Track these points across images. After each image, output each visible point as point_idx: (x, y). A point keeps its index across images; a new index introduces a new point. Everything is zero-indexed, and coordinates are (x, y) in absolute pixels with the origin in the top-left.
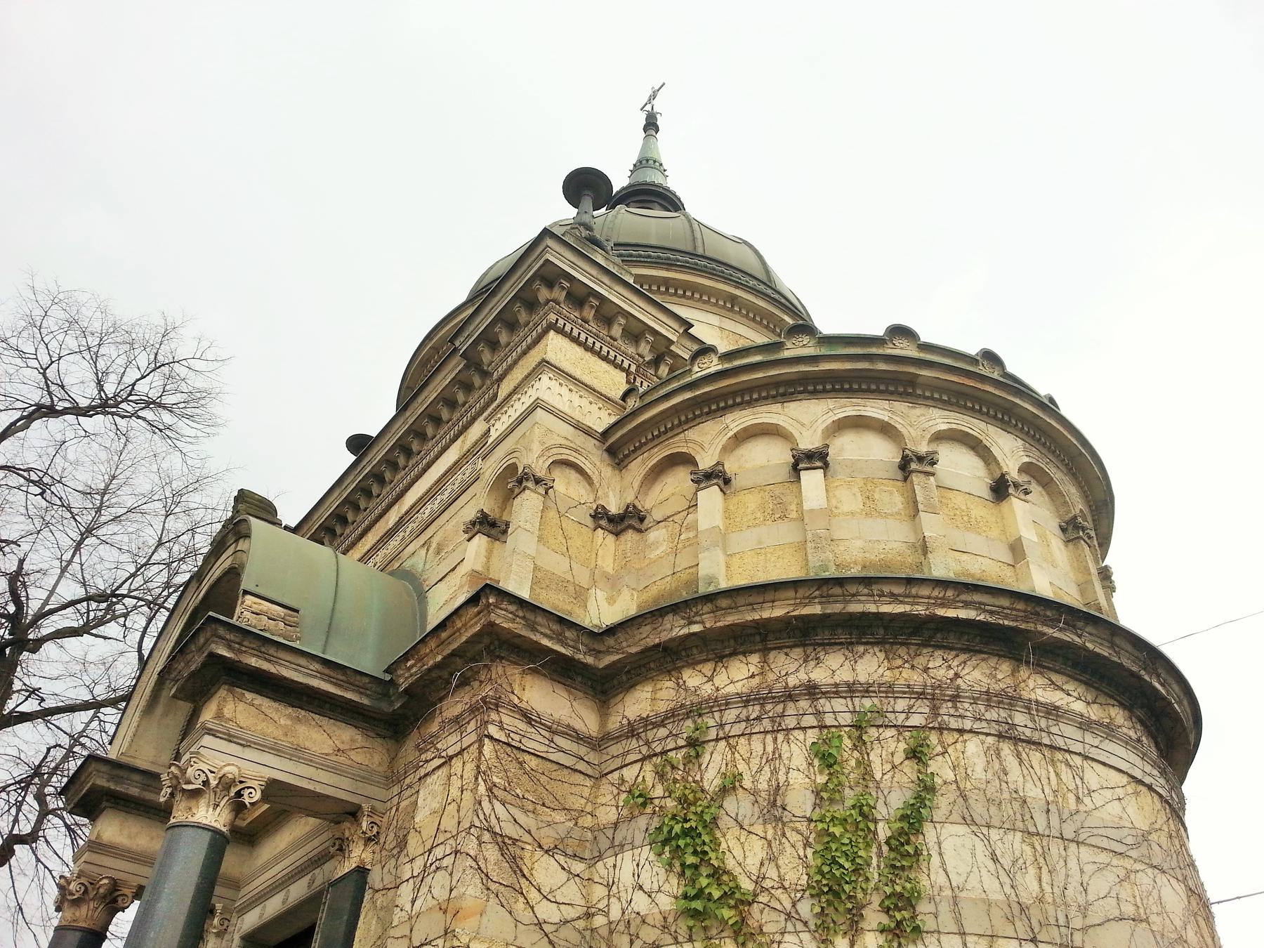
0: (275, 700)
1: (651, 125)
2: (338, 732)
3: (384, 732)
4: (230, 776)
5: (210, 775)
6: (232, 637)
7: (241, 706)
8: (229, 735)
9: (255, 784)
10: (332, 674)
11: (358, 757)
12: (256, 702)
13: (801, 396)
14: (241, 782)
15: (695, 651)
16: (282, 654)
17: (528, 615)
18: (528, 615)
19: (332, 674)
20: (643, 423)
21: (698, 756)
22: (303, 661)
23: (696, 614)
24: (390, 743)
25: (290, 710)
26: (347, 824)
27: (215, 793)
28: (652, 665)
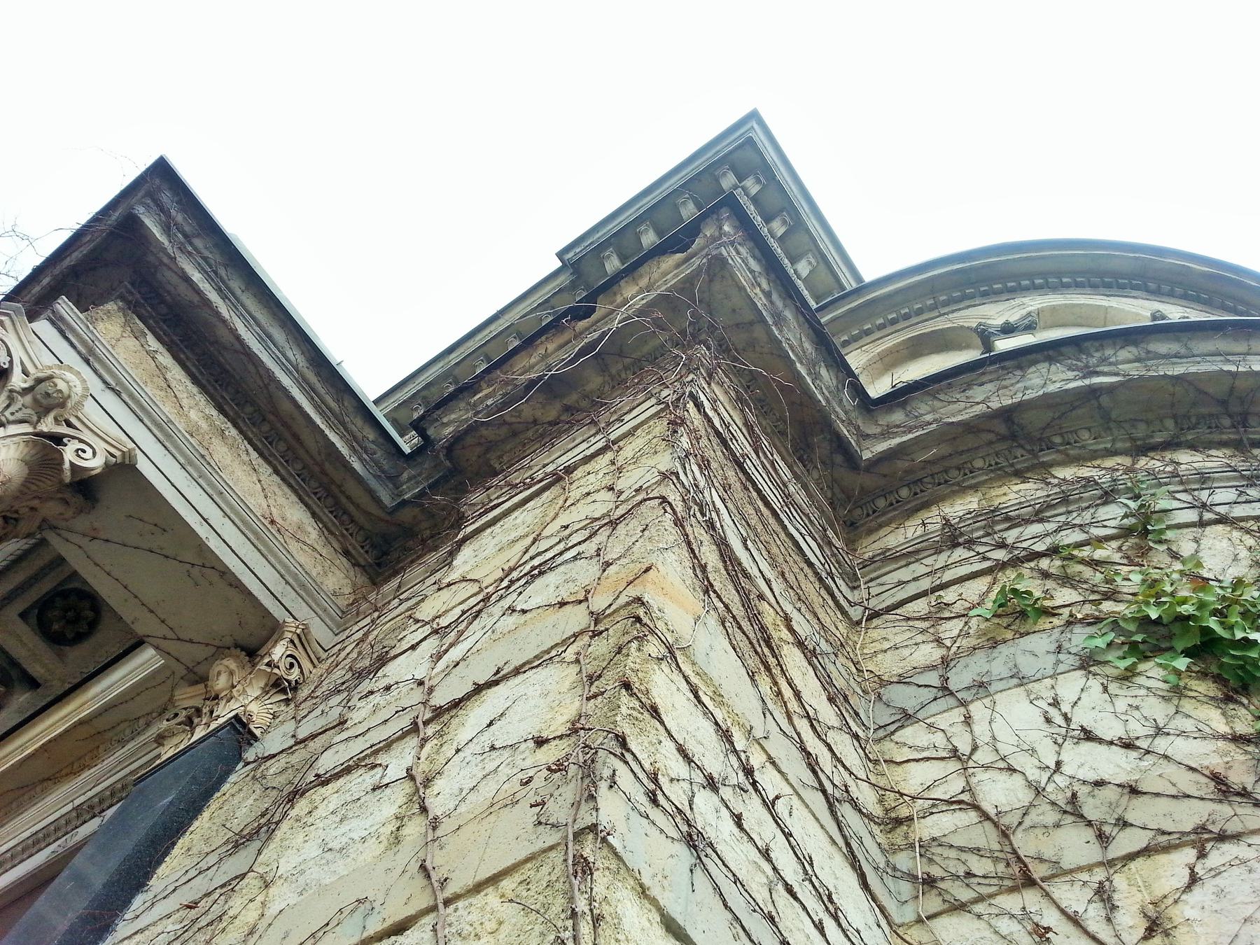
0: (195, 381)
1: (562, 604)
2: (281, 500)
3: (358, 552)
4: (61, 385)
5: (17, 370)
6: (179, 218)
7: (131, 343)
8: (91, 351)
9: (100, 446)
10: (318, 386)
11: (304, 558)
12: (160, 358)
13: (1135, 293)
14: (69, 424)
15: (1085, 435)
16: (250, 302)
17: (775, 297)
18: (775, 297)
19: (318, 386)
20: (873, 301)
21: (934, 839)
22: (279, 335)
23: (1104, 360)
24: (361, 579)
25: (214, 413)
26: (231, 664)
27: (11, 400)
28: (979, 463)
